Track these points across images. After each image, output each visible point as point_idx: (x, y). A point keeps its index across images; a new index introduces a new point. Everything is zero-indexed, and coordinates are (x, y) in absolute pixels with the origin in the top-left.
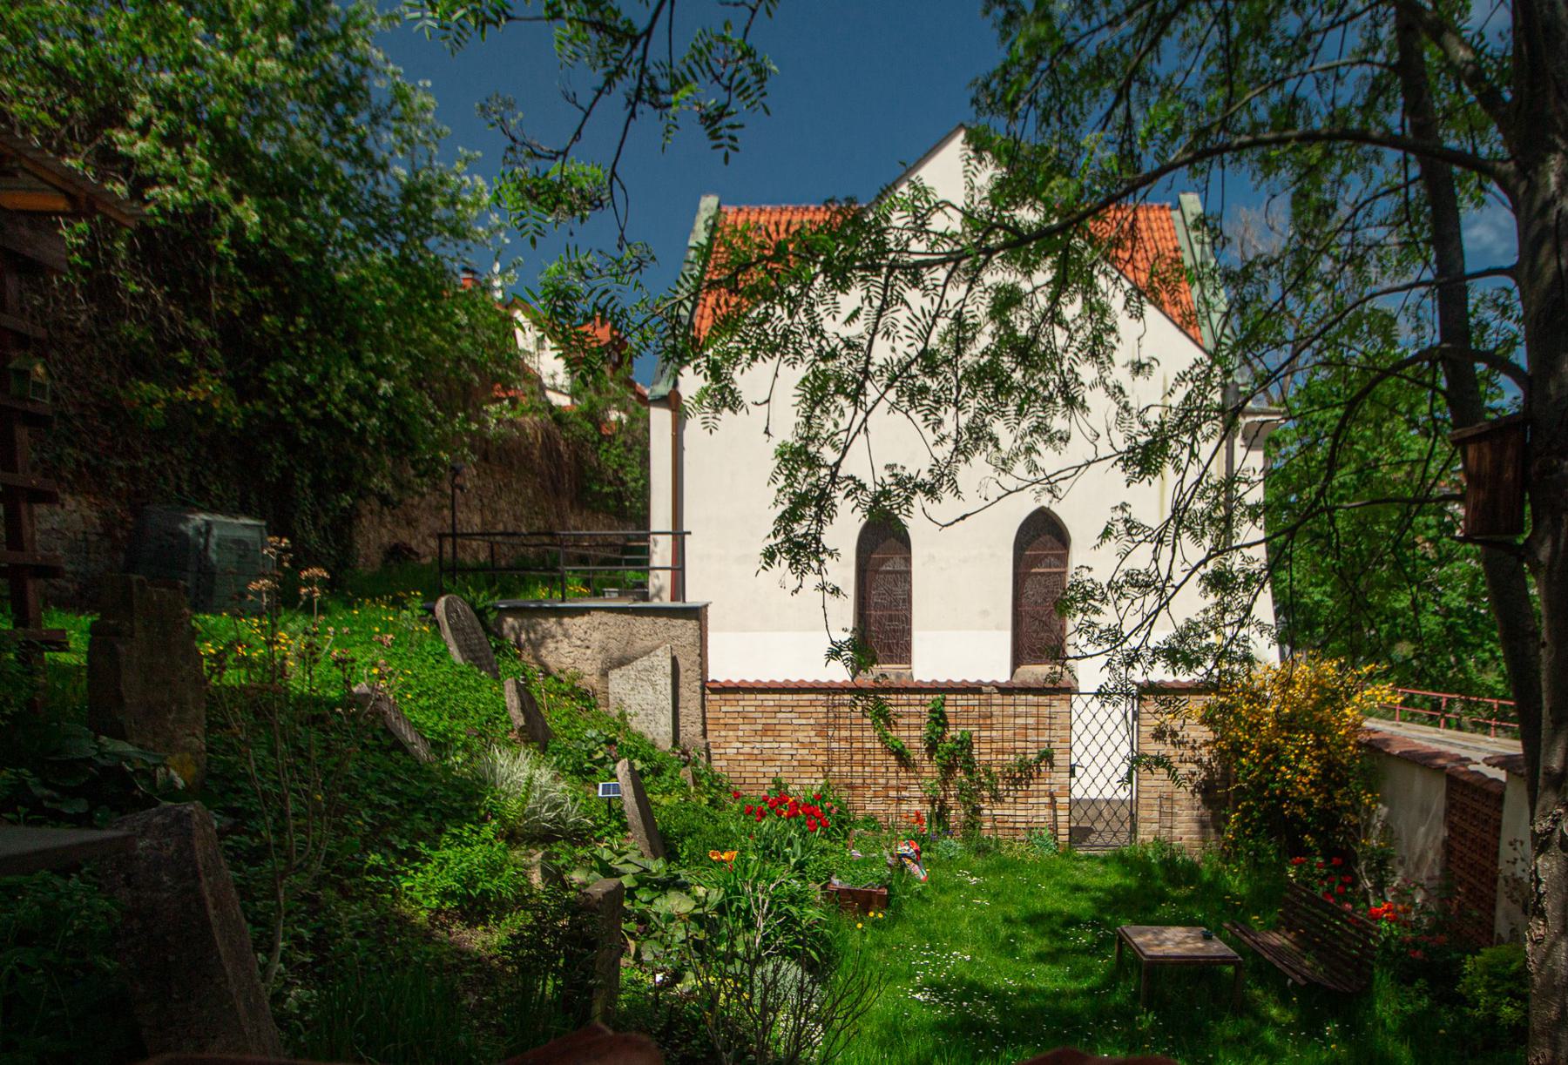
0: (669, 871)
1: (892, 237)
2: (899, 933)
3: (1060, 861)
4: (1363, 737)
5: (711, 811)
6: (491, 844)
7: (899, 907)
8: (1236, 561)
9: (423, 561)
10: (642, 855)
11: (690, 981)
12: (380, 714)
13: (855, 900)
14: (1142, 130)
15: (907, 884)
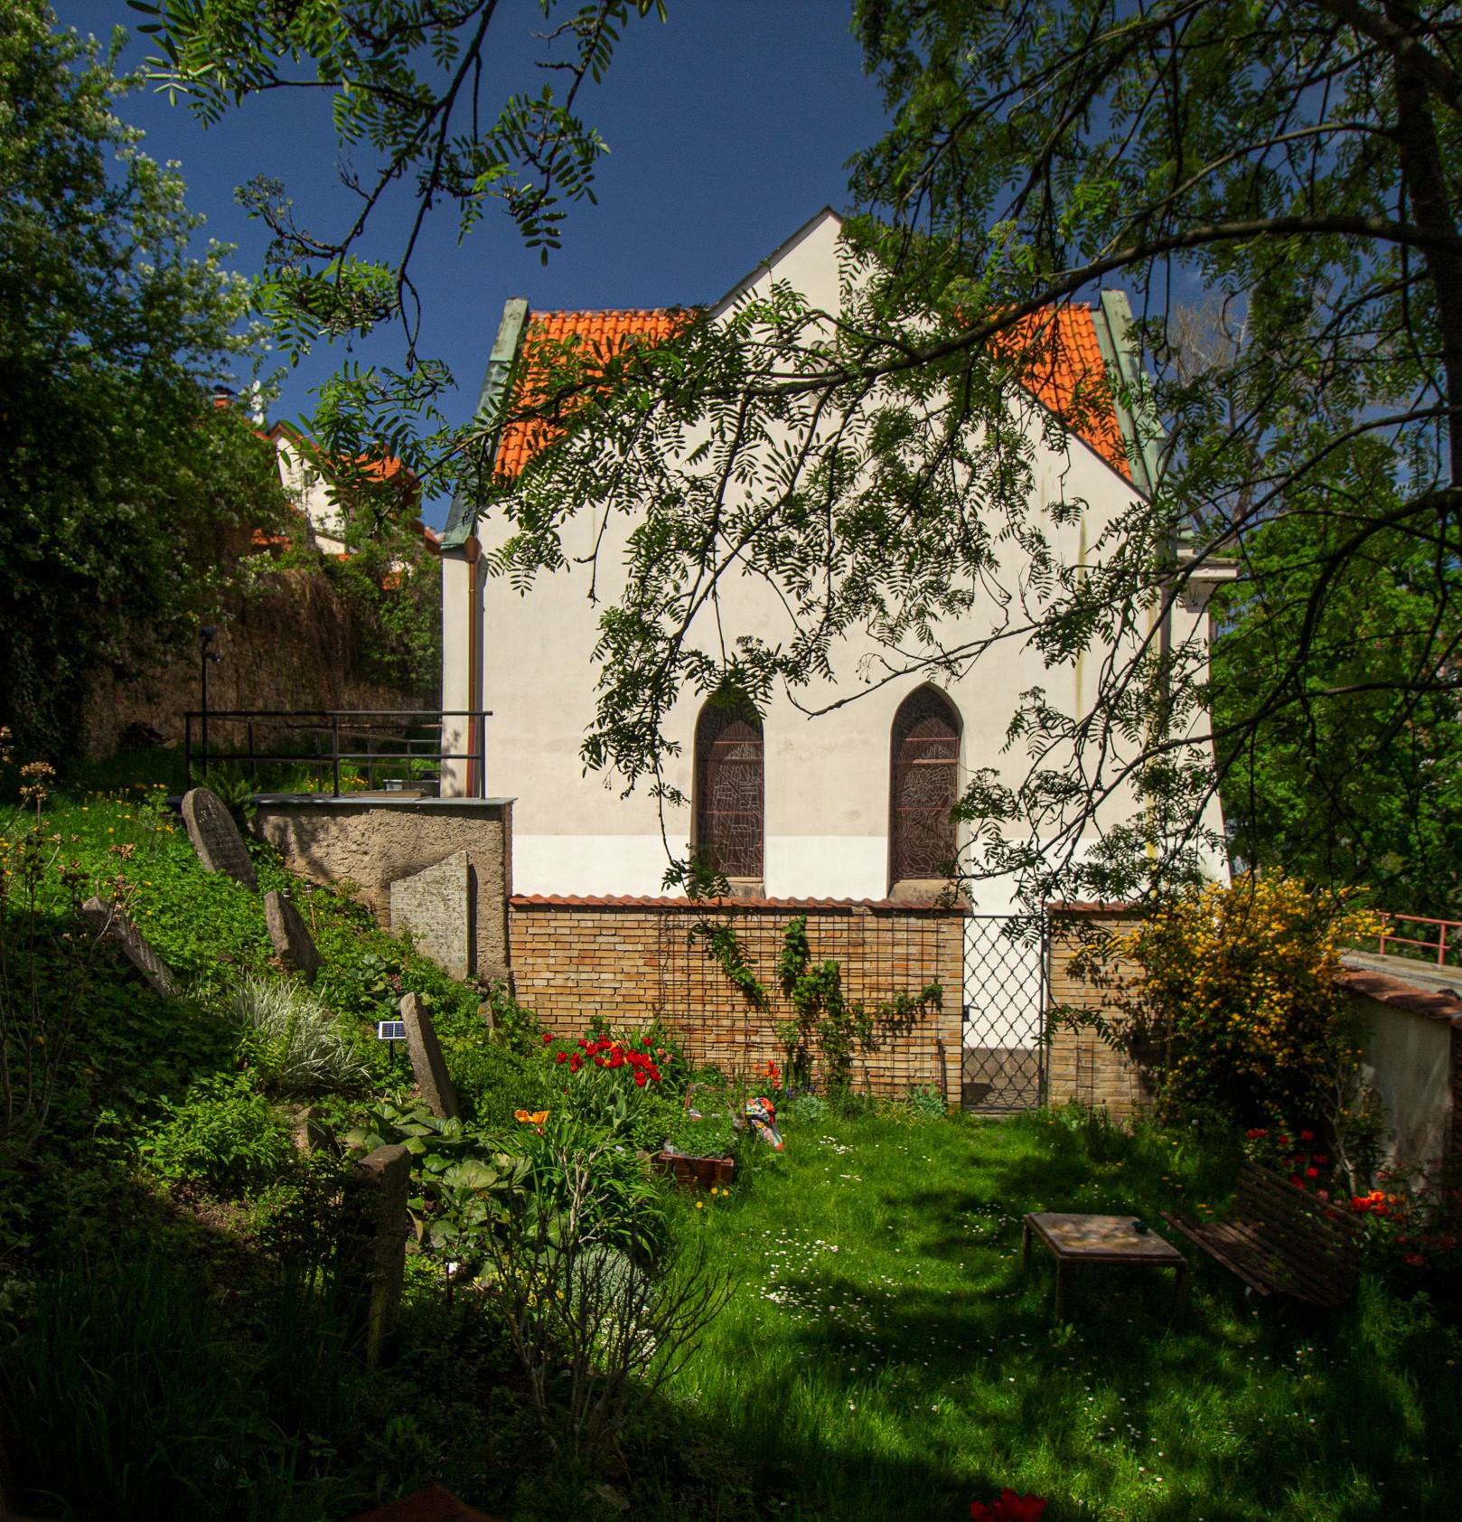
0: (464, 1133)
1: (750, 355)
2: (748, 1216)
3: (950, 1127)
4: (1343, 978)
5: (515, 1057)
6: (248, 1099)
7: (748, 1183)
8: (1181, 757)
9: (167, 745)
10: (432, 1113)
11: (490, 1275)
12: (119, 943)
13: (693, 1173)
14: (1065, 216)
15: (759, 1153)
